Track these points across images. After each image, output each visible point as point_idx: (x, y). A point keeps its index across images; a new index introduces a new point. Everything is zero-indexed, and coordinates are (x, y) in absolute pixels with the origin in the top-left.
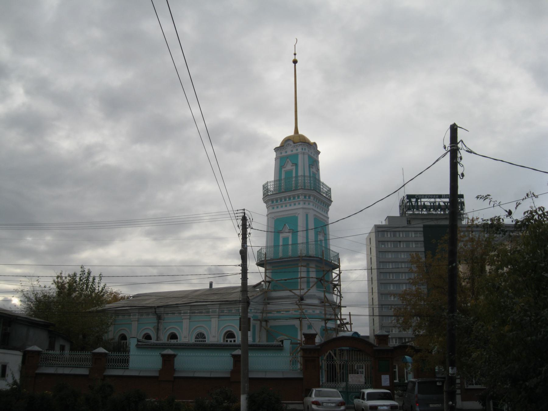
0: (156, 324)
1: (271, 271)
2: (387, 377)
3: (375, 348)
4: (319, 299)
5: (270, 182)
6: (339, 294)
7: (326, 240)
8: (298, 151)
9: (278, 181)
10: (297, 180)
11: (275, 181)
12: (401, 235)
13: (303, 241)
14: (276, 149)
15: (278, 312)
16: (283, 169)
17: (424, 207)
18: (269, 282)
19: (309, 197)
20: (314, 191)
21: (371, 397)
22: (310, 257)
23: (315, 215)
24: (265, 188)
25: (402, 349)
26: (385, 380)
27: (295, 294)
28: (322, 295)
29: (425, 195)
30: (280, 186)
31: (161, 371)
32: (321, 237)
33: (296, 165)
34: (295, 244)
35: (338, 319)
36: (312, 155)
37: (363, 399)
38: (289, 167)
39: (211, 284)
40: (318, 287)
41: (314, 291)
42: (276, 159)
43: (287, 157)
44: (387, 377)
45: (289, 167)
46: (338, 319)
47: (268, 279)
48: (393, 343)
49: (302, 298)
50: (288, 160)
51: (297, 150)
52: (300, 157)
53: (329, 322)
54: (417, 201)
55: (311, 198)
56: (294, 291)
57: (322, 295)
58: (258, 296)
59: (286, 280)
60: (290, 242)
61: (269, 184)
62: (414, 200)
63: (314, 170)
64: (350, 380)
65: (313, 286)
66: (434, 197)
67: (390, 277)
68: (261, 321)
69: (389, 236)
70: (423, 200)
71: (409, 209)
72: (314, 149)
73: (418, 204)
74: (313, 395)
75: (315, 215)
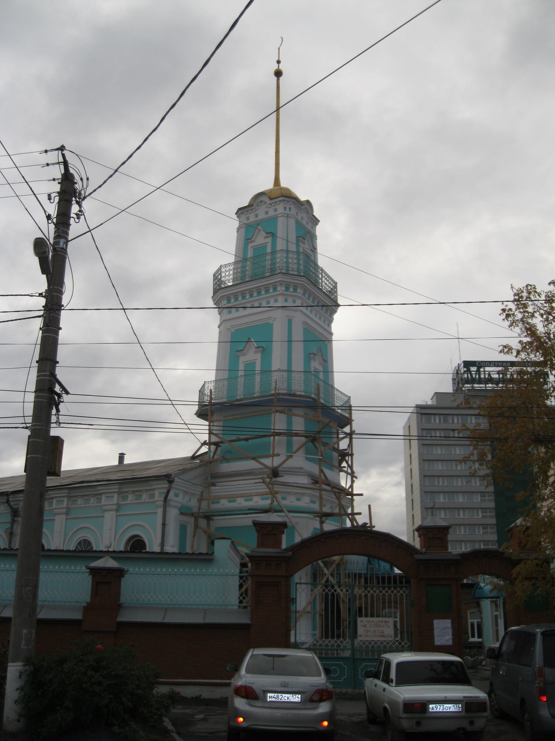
0: (9, 526)
1: (221, 424)
2: (448, 623)
3: (417, 557)
4: (311, 476)
5: (226, 265)
6: (349, 471)
7: (328, 370)
8: (278, 212)
9: (241, 261)
10: (273, 259)
11: (235, 263)
12: (456, 421)
13: (283, 365)
14: (241, 212)
15: (232, 498)
16: (250, 245)
17: (490, 380)
18: (217, 444)
19: (295, 290)
20: (304, 279)
21: (410, 674)
22: (294, 395)
23: (305, 323)
24: (217, 278)
25: (480, 560)
26: (443, 630)
27: (266, 467)
28: (314, 469)
29: (490, 362)
30: (243, 272)
31: (88, 609)
32: (315, 365)
33: (273, 235)
34: (266, 371)
35: (348, 515)
36: (304, 222)
37: (387, 680)
38: (260, 239)
39: (121, 457)
40: (307, 452)
41: (299, 461)
42: (238, 229)
43: (258, 223)
44: (448, 623)
45: (260, 239)
46: (348, 515)
47: (214, 439)
48: (456, 548)
49: (275, 473)
50: (259, 228)
51: (276, 210)
52: (281, 222)
53: (329, 518)
54: (478, 371)
55: (299, 290)
56: (262, 460)
57: (314, 469)
58: (191, 469)
59: (247, 440)
60: (258, 367)
61: (223, 270)
62: (473, 369)
63: (306, 246)
64: (360, 630)
65: (298, 450)
66: (509, 364)
67: (439, 483)
68: (196, 516)
69: (437, 421)
70: (487, 369)
71: (467, 381)
72: (308, 213)
73: (479, 376)
74: (243, 671)
75: (305, 323)
